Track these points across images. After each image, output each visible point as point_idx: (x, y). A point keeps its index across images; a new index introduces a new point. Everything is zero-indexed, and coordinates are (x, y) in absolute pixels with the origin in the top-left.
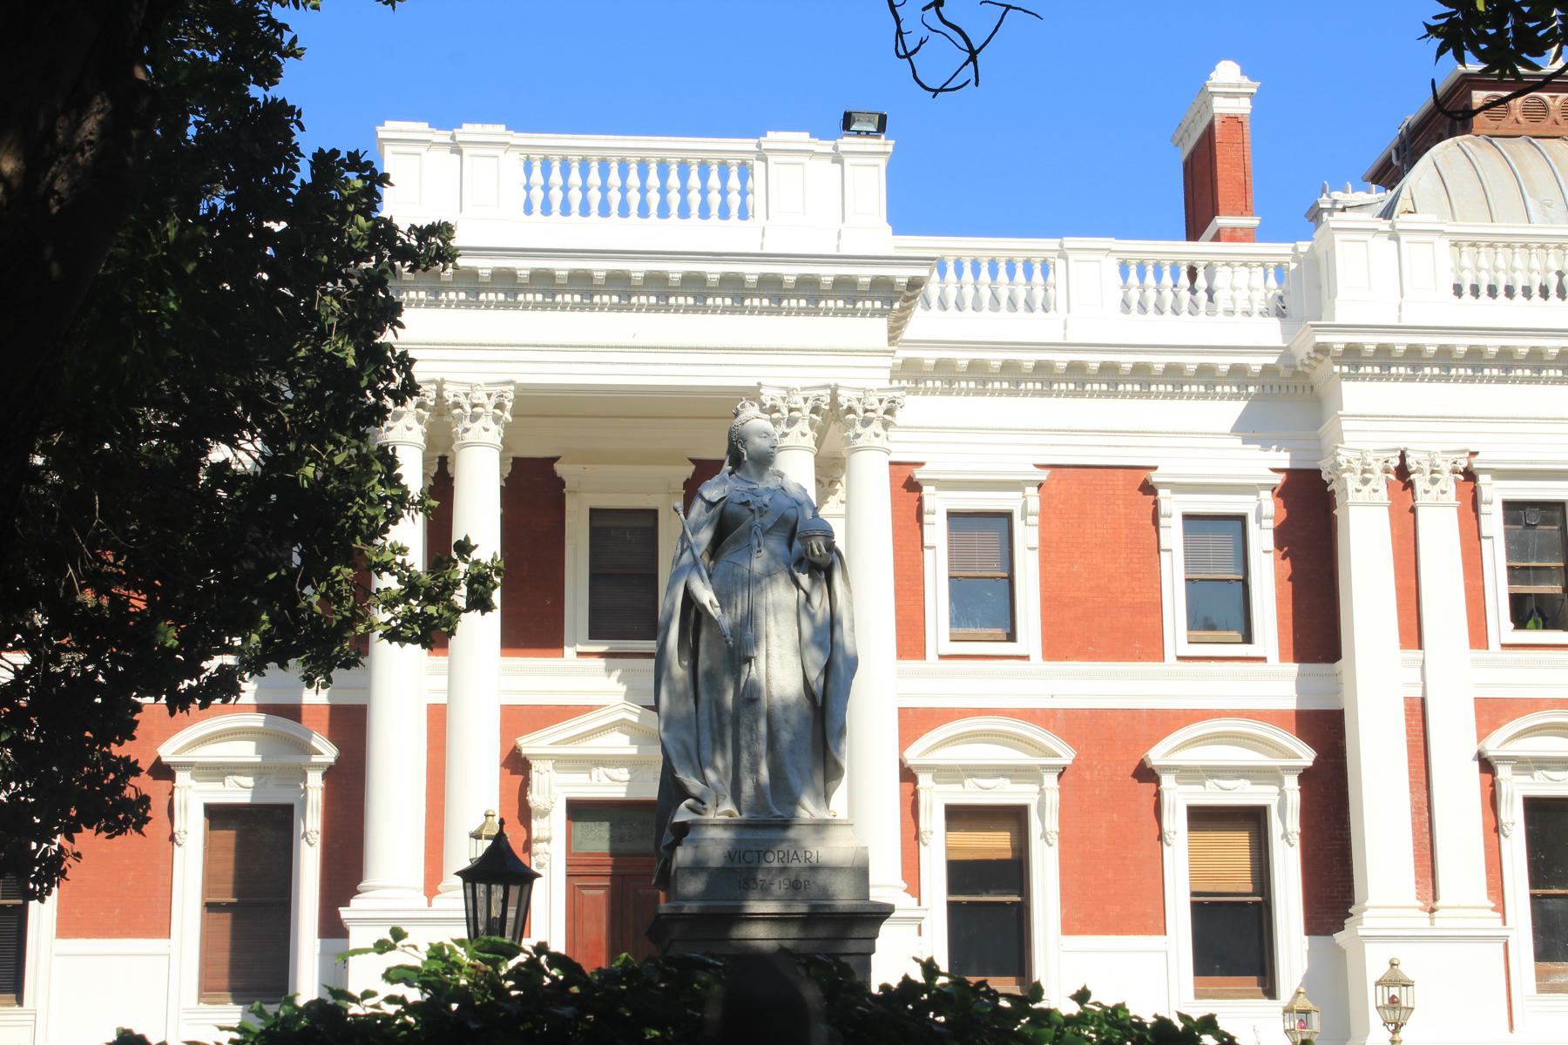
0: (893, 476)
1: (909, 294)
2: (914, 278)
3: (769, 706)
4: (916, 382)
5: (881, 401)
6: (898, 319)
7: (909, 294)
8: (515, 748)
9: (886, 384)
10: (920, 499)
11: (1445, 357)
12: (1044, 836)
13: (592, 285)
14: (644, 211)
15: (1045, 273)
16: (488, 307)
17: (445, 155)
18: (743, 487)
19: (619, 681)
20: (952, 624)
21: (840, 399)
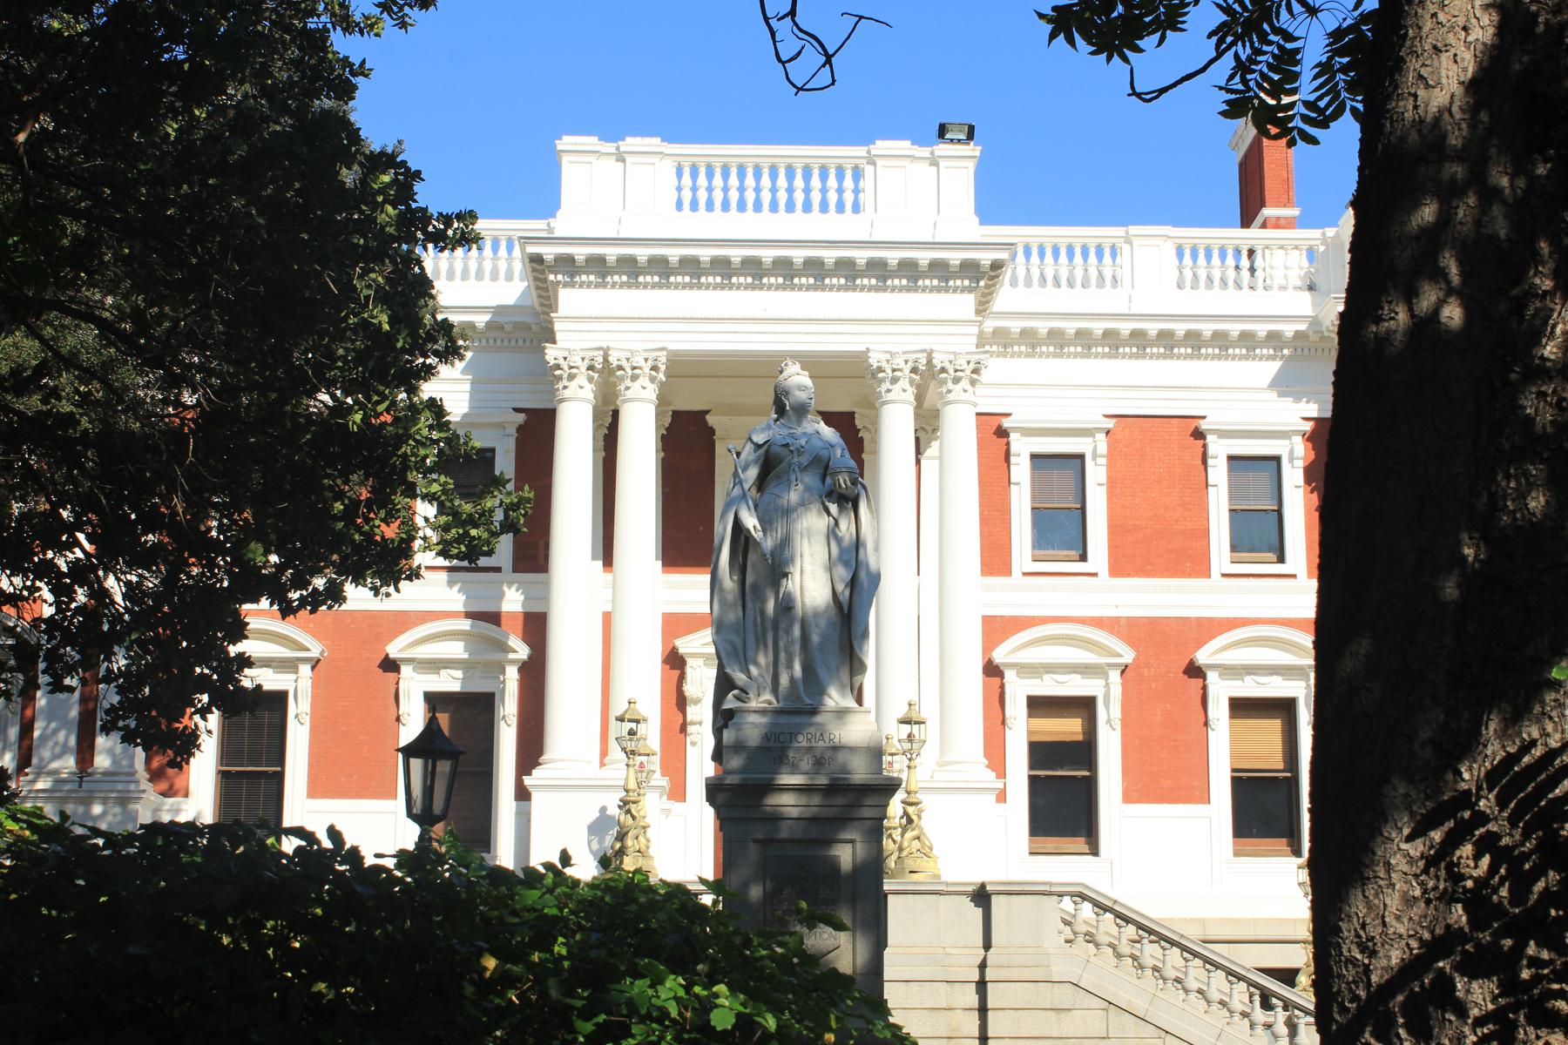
0: (980, 428)
1: (993, 274)
2: (996, 260)
3: (804, 613)
4: (1005, 347)
5: (969, 362)
6: (984, 295)
7: (993, 274)
8: (674, 648)
9: (975, 350)
10: (1008, 444)
12: (1109, 722)
13: (699, 268)
14: (774, 207)
15: (1114, 255)
16: (645, 287)
17: (611, 163)
18: (785, 431)
19: (459, 592)
20: (1034, 547)
21: (934, 361)
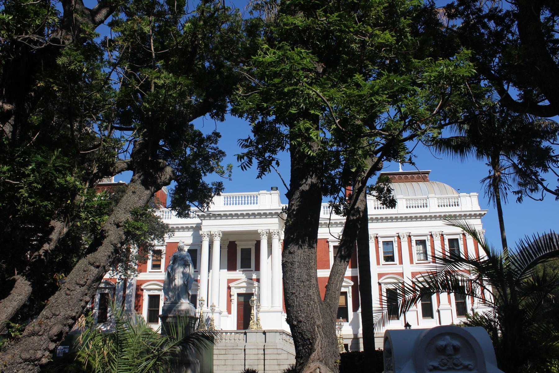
11: (406, 218)
14: (233, 204)
